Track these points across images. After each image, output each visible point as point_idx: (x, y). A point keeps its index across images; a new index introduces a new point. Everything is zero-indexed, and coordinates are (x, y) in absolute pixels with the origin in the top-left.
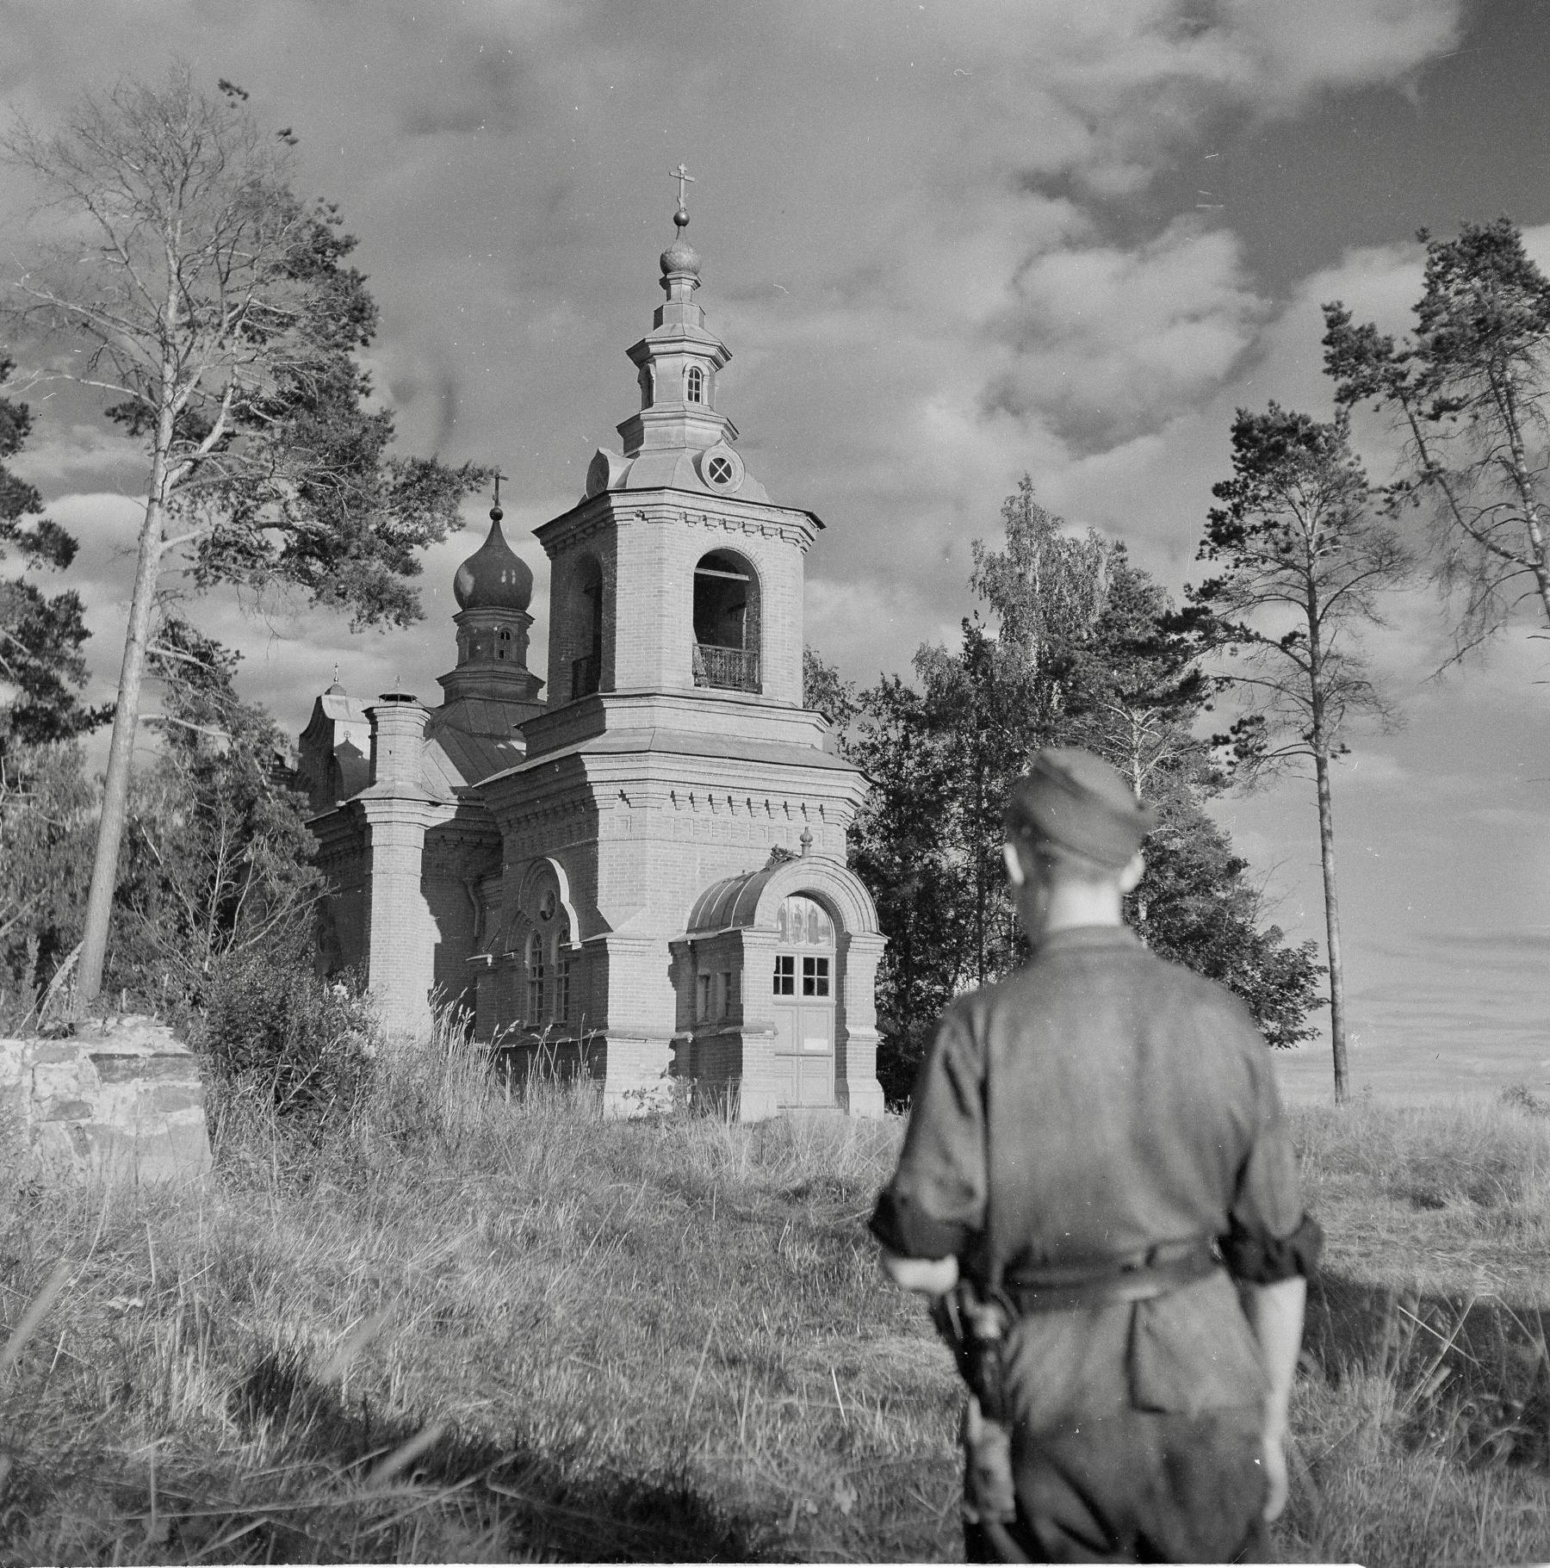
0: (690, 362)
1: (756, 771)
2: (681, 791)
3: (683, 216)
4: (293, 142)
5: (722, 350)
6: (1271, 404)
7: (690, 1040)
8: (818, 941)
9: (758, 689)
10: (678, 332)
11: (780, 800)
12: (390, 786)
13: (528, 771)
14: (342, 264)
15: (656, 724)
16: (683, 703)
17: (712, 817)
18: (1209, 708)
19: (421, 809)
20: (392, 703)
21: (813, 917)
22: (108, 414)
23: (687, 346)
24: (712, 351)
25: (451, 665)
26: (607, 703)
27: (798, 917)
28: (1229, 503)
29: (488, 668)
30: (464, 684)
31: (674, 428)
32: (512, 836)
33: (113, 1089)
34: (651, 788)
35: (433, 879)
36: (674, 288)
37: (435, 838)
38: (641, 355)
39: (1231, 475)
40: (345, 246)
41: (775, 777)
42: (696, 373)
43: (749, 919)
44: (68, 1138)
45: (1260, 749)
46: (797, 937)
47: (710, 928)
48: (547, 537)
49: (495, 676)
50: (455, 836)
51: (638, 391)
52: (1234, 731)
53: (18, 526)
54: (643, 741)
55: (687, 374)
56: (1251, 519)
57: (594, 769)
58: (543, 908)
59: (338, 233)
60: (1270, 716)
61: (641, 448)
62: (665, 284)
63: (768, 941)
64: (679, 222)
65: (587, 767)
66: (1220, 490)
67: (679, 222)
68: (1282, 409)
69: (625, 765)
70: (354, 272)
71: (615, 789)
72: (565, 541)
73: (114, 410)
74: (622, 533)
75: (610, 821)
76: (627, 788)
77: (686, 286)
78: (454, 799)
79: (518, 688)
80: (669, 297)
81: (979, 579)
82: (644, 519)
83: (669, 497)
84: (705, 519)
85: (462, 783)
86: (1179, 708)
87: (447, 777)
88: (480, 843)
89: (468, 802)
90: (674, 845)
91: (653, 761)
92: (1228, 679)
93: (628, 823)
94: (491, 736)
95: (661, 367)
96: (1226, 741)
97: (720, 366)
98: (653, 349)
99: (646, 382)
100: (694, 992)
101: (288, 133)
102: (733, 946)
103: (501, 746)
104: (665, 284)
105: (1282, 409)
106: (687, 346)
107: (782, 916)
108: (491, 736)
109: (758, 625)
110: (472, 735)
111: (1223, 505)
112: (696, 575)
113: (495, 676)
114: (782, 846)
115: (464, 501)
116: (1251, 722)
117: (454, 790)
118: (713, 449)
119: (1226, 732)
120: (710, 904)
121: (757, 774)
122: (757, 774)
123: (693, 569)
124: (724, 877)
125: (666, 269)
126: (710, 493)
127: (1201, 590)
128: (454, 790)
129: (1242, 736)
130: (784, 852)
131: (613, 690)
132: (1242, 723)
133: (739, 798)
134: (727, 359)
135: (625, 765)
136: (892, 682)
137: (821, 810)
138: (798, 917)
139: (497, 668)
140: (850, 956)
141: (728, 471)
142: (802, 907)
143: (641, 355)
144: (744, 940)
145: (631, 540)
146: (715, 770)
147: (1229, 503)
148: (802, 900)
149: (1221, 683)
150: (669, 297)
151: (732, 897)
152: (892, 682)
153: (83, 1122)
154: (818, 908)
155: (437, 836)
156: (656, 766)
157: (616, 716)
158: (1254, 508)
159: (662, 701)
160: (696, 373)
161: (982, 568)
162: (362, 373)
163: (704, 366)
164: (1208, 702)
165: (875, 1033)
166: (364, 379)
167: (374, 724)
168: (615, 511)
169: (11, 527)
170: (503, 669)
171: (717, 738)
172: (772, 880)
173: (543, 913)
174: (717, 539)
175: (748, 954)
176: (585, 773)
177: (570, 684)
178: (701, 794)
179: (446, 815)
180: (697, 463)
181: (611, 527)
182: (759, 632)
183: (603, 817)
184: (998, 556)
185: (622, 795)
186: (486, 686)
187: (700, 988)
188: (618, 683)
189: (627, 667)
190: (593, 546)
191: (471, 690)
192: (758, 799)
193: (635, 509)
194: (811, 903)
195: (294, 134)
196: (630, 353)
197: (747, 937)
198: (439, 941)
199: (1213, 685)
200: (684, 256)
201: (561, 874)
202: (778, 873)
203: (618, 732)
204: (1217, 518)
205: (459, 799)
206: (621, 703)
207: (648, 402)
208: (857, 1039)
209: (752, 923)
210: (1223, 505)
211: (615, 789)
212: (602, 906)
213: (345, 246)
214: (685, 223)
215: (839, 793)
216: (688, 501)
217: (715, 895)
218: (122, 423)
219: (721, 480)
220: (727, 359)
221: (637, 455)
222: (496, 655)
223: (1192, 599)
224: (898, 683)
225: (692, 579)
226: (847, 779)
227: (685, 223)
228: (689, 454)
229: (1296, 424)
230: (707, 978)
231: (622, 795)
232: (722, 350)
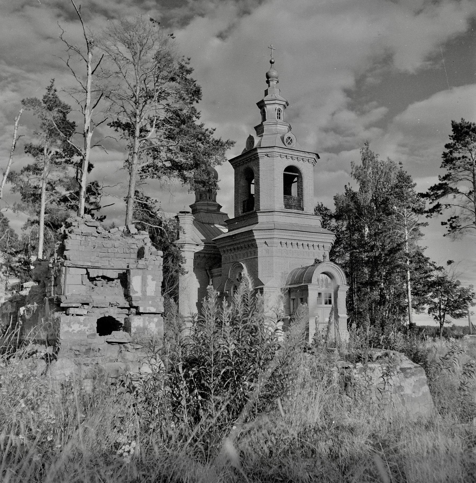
0: (278, 107)
1: (305, 235)
2: (283, 241)
3: (273, 61)
4: (173, 38)
5: (287, 103)
6: (462, 119)
7: (289, 319)
8: (328, 288)
9: (303, 210)
10: (273, 97)
11: (296, 242)
12: (184, 240)
13: (233, 235)
14: (188, 77)
15: (274, 220)
16: (282, 214)
17: (292, 249)
18: (441, 214)
19: (194, 247)
20: (184, 214)
21: (326, 280)
22: (108, 125)
23: (277, 102)
24: (284, 103)
25: (193, 202)
26: (258, 214)
27: (322, 280)
28: (449, 150)
29: (206, 202)
30: (198, 207)
31: (273, 127)
32: (225, 255)
33: (408, 380)
34: (275, 240)
35: (197, 267)
36: (271, 83)
37: (197, 256)
38: (261, 105)
39: (452, 141)
40: (189, 72)
41: (311, 236)
42: (279, 110)
43: (310, 281)
44: (399, 399)
45: (459, 226)
46: (322, 286)
47: (294, 284)
48: (233, 163)
49: (208, 205)
50: (203, 255)
51: (260, 117)
52: (449, 220)
53: (72, 160)
54: (272, 226)
55: (277, 110)
56: (456, 155)
57: (257, 235)
58: (237, 277)
59: (188, 67)
60: (462, 216)
61: (263, 134)
62: (268, 82)
63: (315, 288)
64: (271, 63)
65: (255, 234)
66: (447, 146)
67: (271, 63)
68: (465, 121)
69: (267, 233)
70: (192, 79)
71: (263, 241)
72: (240, 163)
73: (110, 123)
74: (261, 161)
75: (261, 250)
76: (267, 241)
77: (275, 82)
78: (203, 244)
79: (215, 208)
80: (269, 86)
81: (353, 173)
82: (268, 156)
83: (276, 149)
84: (286, 156)
85: (204, 238)
86: (432, 214)
87: (199, 237)
88: (210, 257)
89: (207, 244)
90: (282, 258)
91: (276, 232)
92: (449, 205)
93: (267, 251)
94: (209, 224)
95: (268, 108)
96: (446, 224)
97: (285, 108)
98: (266, 102)
99: (263, 114)
100: (289, 304)
101: (172, 35)
102: (305, 290)
103: (212, 226)
104: (268, 82)
105: (465, 121)
106: (277, 102)
107: (318, 280)
108: (209, 224)
109: (302, 189)
110: (203, 223)
111: (447, 151)
112: (284, 174)
113: (208, 205)
114: (318, 259)
115: (226, 152)
116: (455, 217)
117: (202, 240)
118: (287, 134)
119: (446, 221)
120: (294, 276)
121: (305, 236)
122: (305, 236)
123: (283, 172)
124: (297, 267)
125: (268, 77)
126: (286, 147)
127: (443, 177)
128: (202, 240)
129: (451, 222)
130: (318, 260)
131: (259, 210)
132: (452, 218)
133: (300, 243)
134: (288, 105)
135: (267, 233)
136: (320, 204)
137: (323, 246)
138: (322, 280)
139: (209, 202)
140: (339, 292)
141: (291, 140)
142: (323, 277)
143: (261, 105)
144: (309, 288)
145: (264, 162)
146: (293, 235)
147: (449, 150)
148: (323, 275)
149: (447, 206)
150: (269, 86)
151: (302, 274)
152: (320, 204)
153: (402, 393)
154: (328, 277)
155: (198, 255)
156: (276, 234)
157: (261, 218)
158: (456, 152)
159: (276, 213)
160: (279, 110)
161: (354, 170)
162: (198, 112)
163: (281, 108)
164: (441, 212)
165: (347, 316)
166: (198, 114)
167: (178, 220)
168: (259, 154)
169: (70, 160)
170: (211, 202)
171: (292, 225)
172: (316, 269)
173: (237, 279)
174: (290, 162)
175: (310, 292)
176: (254, 236)
177: (242, 208)
178: (289, 242)
179: (201, 248)
180: (282, 139)
181: (258, 159)
182: (302, 191)
183: (259, 250)
184: (359, 166)
185: (265, 243)
186: (206, 208)
187: (292, 302)
188: (261, 208)
189: (264, 203)
190: (251, 165)
191: (201, 209)
192: (305, 243)
193: (265, 153)
194: (326, 276)
195: (174, 36)
196: (258, 104)
197: (310, 287)
198: (199, 287)
199: (444, 207)
200: (274, 73)
201: (244, 266)
202: (318, 267)
203: (262, 223)
204: (445, 155)
205: (205, 243)
206: (263, 214)
207: (264, 119)
208: (341, 318)
209: (311, 282)
210: (447, 151)
211: (263, 241)
212: (260, 277)
213: (189, 72)
214: (273, 63)
215: (328, 241)
216: (281, 151)
217: (296, 272)
218: (112, 128)
219: (289, 143)
220: (288, 105)
221: (262, 136)
222: (208, 198)
223: (440, 180)
224: (322, 205)
225: (283, 175)
226: (331, 236)
227: (273, 63)
228: (279, 136)
229: (470, 125)
230: (294, 299)
231: (265, 243)
232: (287, 103)
